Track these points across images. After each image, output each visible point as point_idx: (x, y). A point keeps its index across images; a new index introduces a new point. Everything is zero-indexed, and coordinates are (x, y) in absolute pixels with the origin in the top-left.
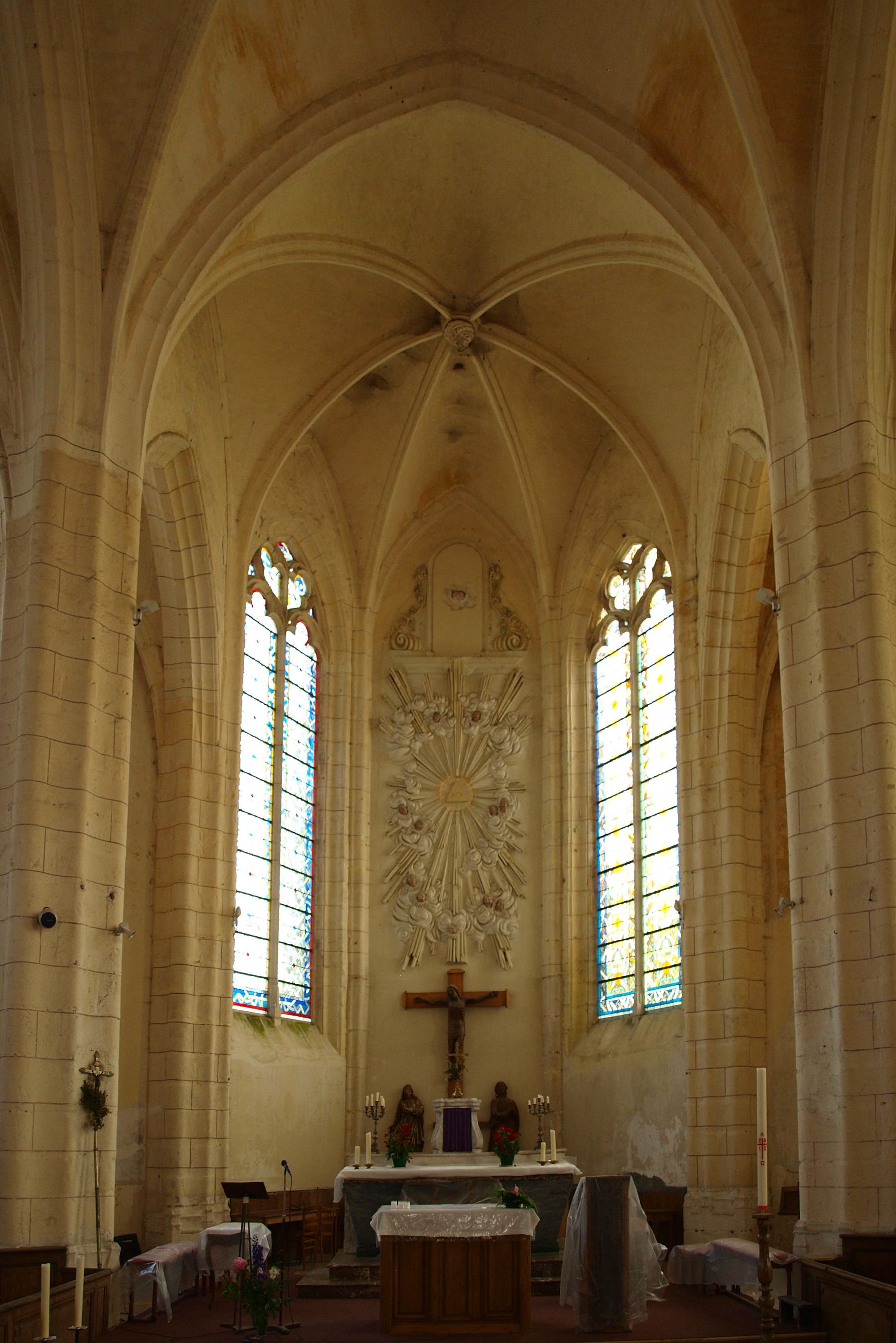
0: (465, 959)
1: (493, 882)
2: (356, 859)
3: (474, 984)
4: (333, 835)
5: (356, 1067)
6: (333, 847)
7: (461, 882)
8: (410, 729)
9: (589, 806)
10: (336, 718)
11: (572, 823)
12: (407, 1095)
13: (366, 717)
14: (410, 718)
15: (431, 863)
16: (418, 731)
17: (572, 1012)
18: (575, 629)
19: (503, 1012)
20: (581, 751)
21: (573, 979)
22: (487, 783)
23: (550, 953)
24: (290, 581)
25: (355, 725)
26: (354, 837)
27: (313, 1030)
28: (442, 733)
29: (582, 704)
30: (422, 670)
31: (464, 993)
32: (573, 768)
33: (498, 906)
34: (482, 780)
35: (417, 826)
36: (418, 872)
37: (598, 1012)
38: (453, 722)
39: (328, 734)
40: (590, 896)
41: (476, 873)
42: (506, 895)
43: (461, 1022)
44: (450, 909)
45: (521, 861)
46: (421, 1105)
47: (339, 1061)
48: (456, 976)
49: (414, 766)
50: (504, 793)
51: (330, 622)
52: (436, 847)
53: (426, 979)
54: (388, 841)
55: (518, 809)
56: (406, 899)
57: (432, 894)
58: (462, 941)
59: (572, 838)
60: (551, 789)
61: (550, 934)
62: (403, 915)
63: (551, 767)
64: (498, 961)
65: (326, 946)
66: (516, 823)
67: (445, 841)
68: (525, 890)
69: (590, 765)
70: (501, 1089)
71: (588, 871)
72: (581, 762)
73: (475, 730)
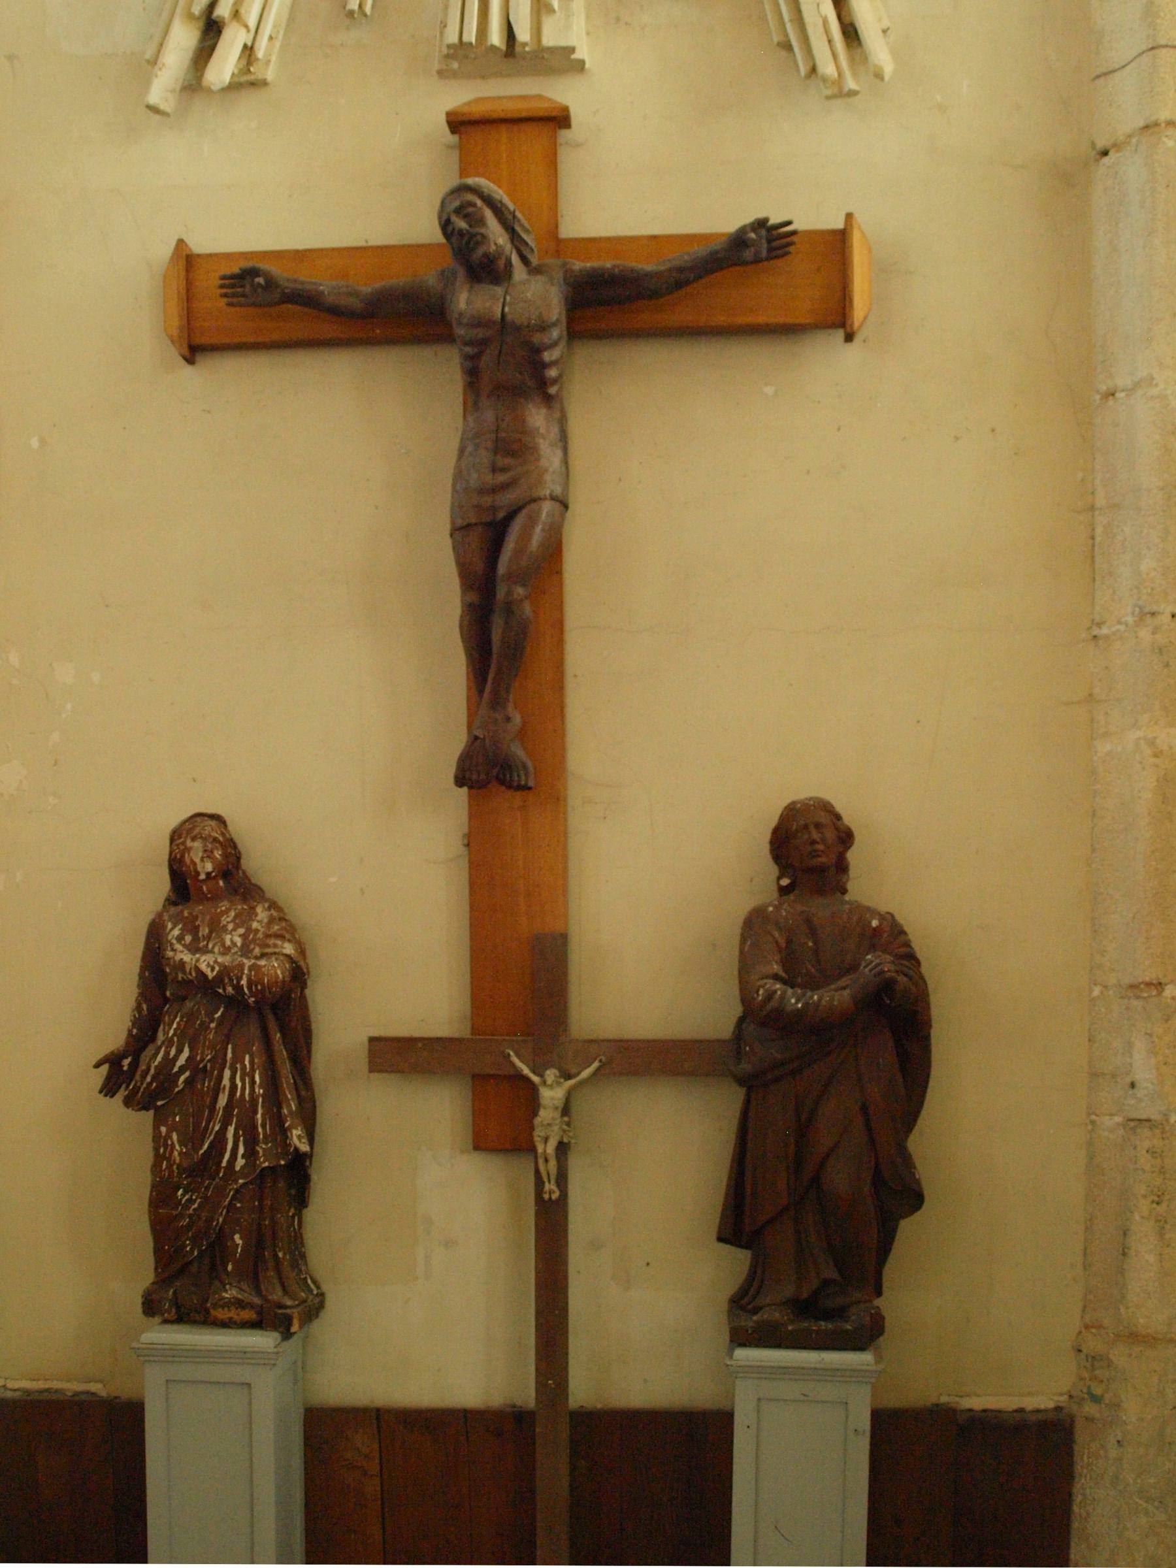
0: (569, 29)
3: (633, 182)
12: (207, 873)
19: (827, 364)
24: (573, 57)
31: (559, 245)
43: (537, 417)
46: (285, 925)
48: (508, 133)
53: (343, 177)
70: (810, 848)
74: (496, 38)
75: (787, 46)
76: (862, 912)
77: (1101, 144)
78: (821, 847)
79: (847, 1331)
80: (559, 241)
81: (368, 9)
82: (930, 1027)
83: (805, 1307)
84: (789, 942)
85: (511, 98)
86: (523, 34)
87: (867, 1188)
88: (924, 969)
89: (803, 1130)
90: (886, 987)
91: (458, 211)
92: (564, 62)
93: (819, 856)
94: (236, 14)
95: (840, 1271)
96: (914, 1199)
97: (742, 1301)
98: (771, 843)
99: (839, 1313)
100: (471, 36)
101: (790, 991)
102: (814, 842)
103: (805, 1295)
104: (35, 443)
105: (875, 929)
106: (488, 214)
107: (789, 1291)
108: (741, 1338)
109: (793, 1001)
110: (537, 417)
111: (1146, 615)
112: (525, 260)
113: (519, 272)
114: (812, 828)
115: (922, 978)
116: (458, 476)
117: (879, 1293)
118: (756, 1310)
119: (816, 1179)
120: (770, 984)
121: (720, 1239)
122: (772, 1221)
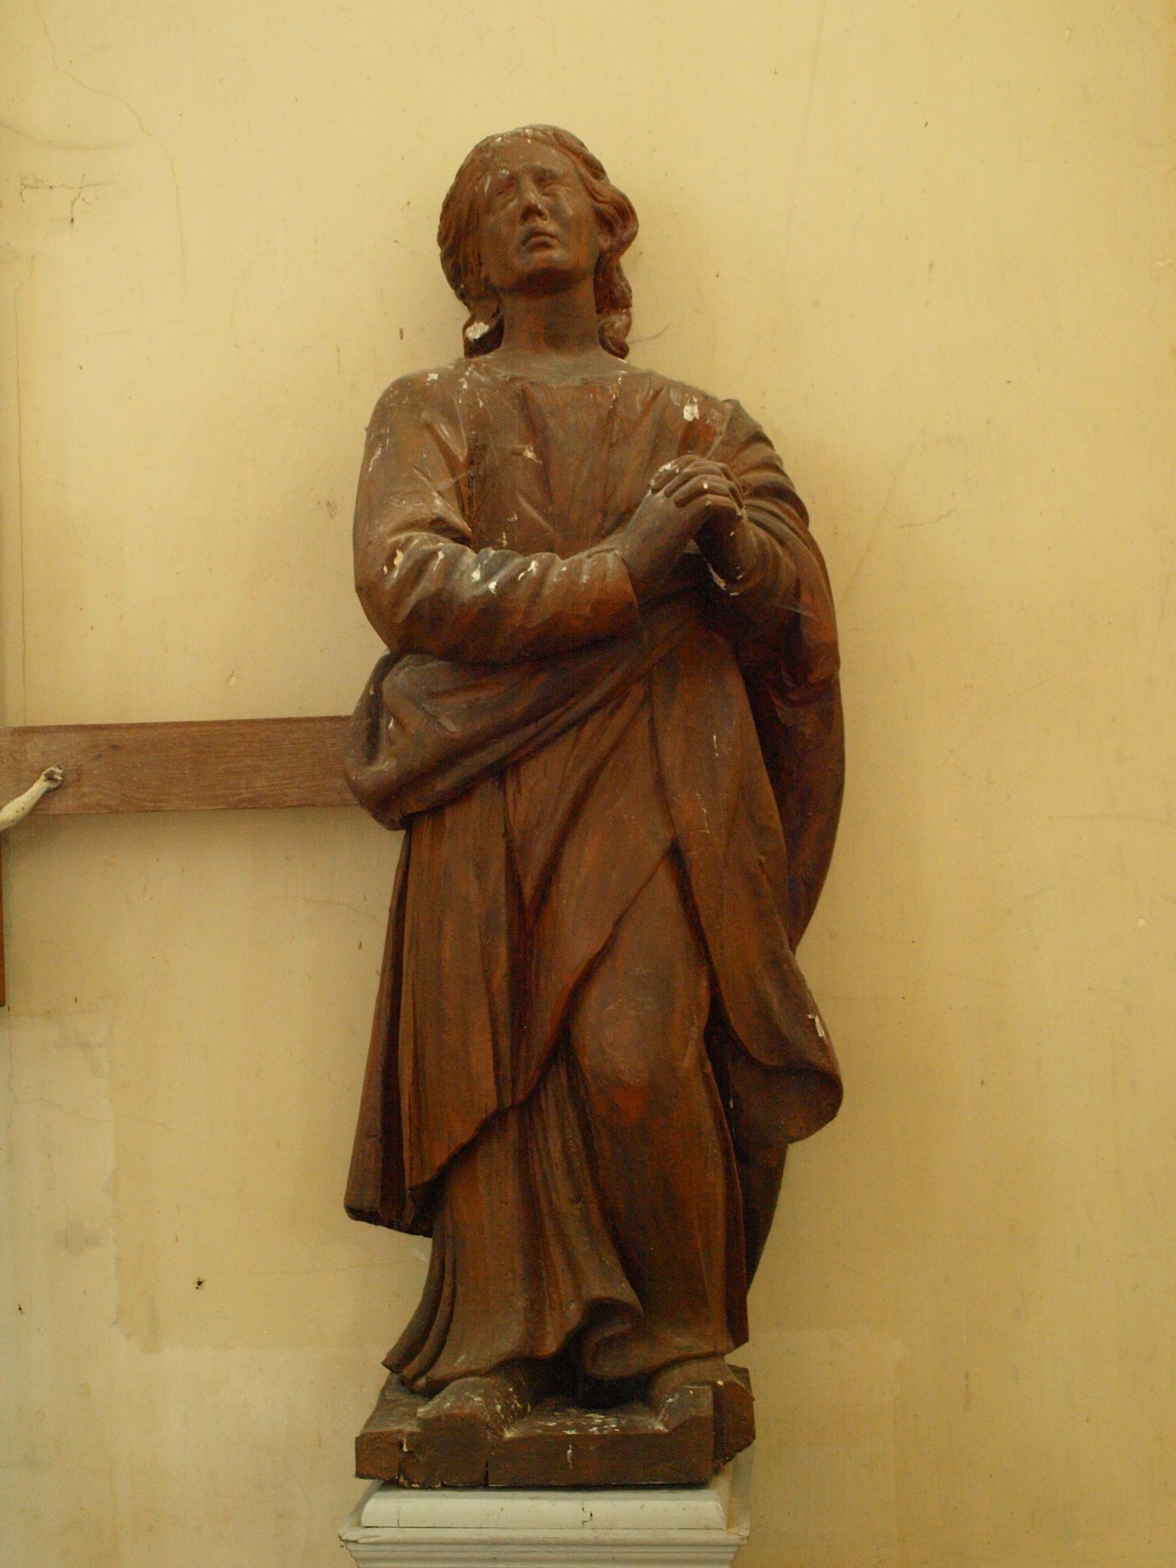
70: (534, 249)
76: (660, 394)
78: (550, 226)
79: (657, 1435)
82: (836, 662)
83: (556, 1376)
84: (477, 452)
87: (689, 1055)
88: (816, 529)
89: (528, 914)
90: (712, 532)
93: (546, 246)
95: (635, 1286)
96: (817, 1089)
97: (414, 1363)
98: (442, 239)
99: (634, 1391)
101: (470, 556)
102: (530, 212)
103: (550, 1346)
105: (691, 425)
107: (507, 1339)
108: (390, 1462)
109: (477, 575)
114: (528, 184)
115: (812, 544)
117: (738, 1332)
118: (433, 1390)
119: (564, 1045)
120: (420, 539)
121: (357, 1212)
122: (465, 1154)
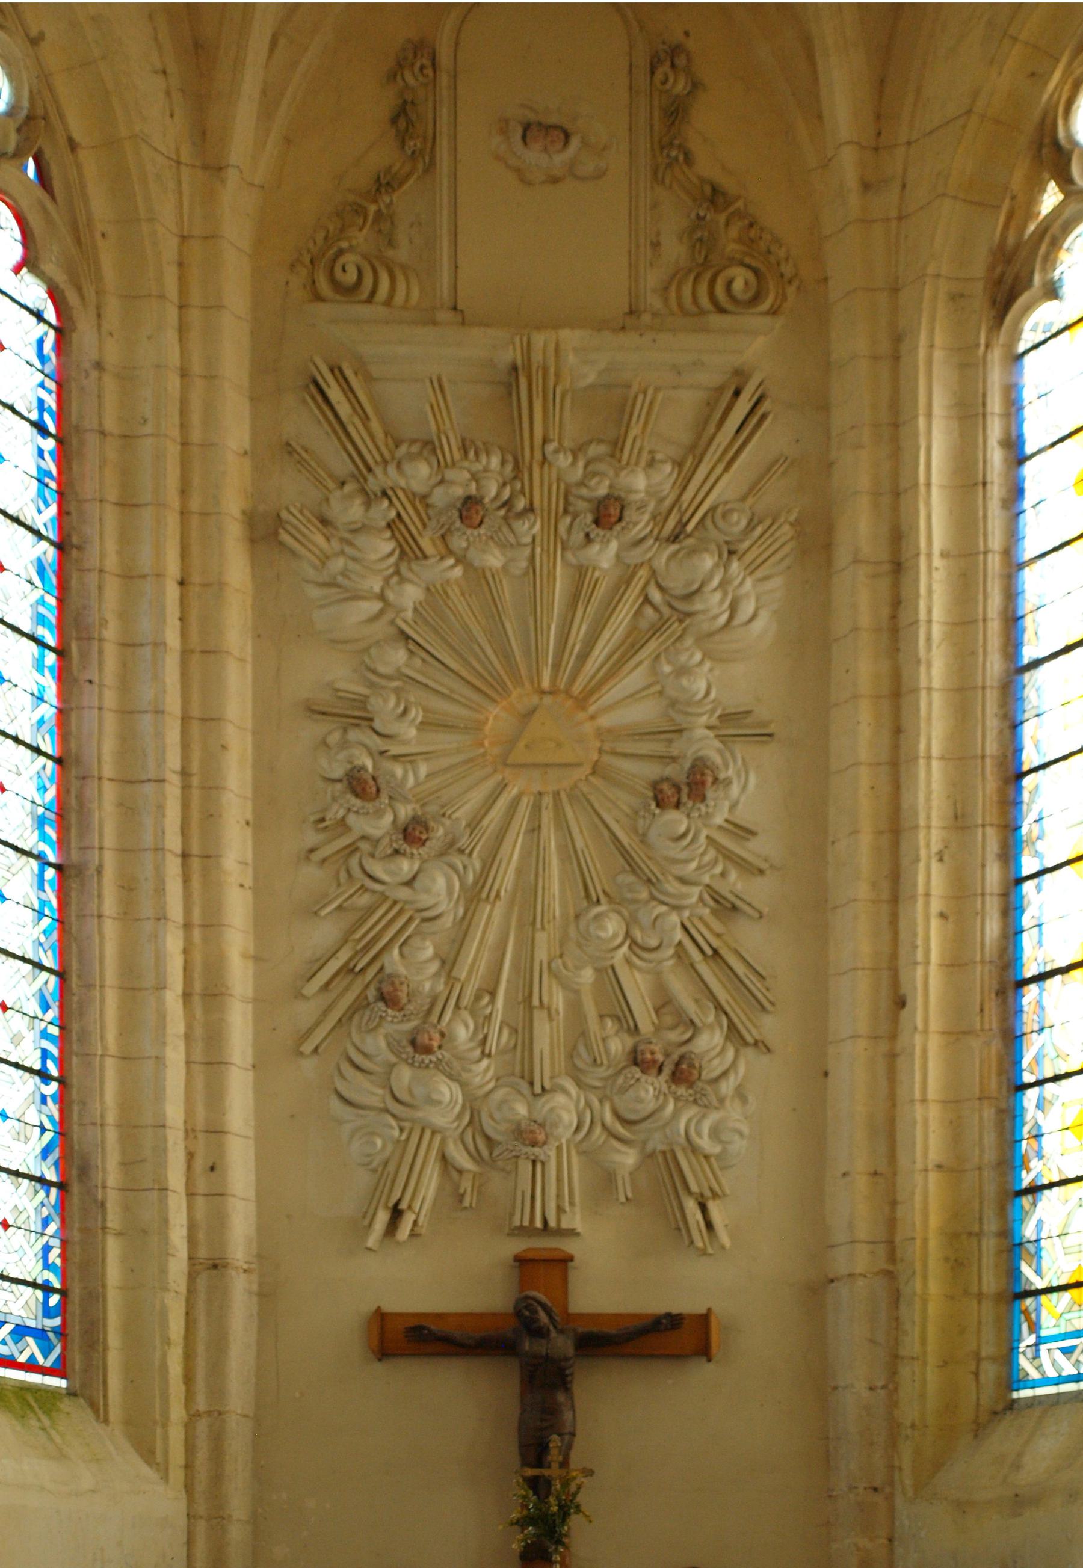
0: (574, 1220)
1: (664, 1003)
2: (205, 924)
3: (607, 1280)
4: (127, 851)
5: (218, 1518)
6: (128, 887)
7: (559, 1000)
8: (381, 546)
9: (990, 784)
10: (127, 505)
11: (931, 831)
13: (233, 504)
14: (383, 512)
15: (460, 941)
16: (408, 552)
17: (925, 1384)
18: (948, 245)
19: (700, 1373)
20: (964, 622)
21: (930, 1285)
22: (644, 712)
23: (853, 1208)
25: (196, 522)
26: (200, 860)
27: (76, 1412)
28: (494, 560)
29: (968, 481)
30: (418, 366)
31: (569, 1317)
32: (935, 669)
33: (682, 1072)
34: (627, 702)
35: (412, 833)
36: (418, 967)
37: (1011, 1379)
38: (528, 529)
39: (104, 548)
40: (984, 1050)
41: (608, 976)
42: (710, 1042)
43: (561, 1397)
44: (526, 1078)
45: (752, 940)
47: (163, 1501)
48: (542, 1267)
49: (398, 656)
50: (703, 742)
51: (100, 206)
52: (475, 895)
53: (453, 1274)
54: (312, 876)
55: (748, 789)
56: (377, 1044)
57: (462, 1034)
58: (564, 1174)
59: (931, 880)
60: (860, 733)
61: (852, 1152)
62: (369, 1092)
63: (862, 667)
64: (681, 1228)
65: (111, 1173)
66: (744, 832)
67: (506, 879)
68: (769, 1027)
69: (995, 666)
71: (982, 977)
72: (965, 655)
73: (605, 555)
74: (539, 1224)
75: (679, 1229)
77: (831, 1276)
80: (569, 1315)
81: (474, 1205)
85: (544, 1249)
86: (552, 1223)
91: (526, 1307)
92: (572, 1233)
94: (410, 1207)
100: (526, 1223)
104: (297, 1395)
106: (539, 1309)
110: (561, 1397)
111: (852, 1488)
112: (555, 1327)
113: (553, 1334)
116: (522, 1423)
